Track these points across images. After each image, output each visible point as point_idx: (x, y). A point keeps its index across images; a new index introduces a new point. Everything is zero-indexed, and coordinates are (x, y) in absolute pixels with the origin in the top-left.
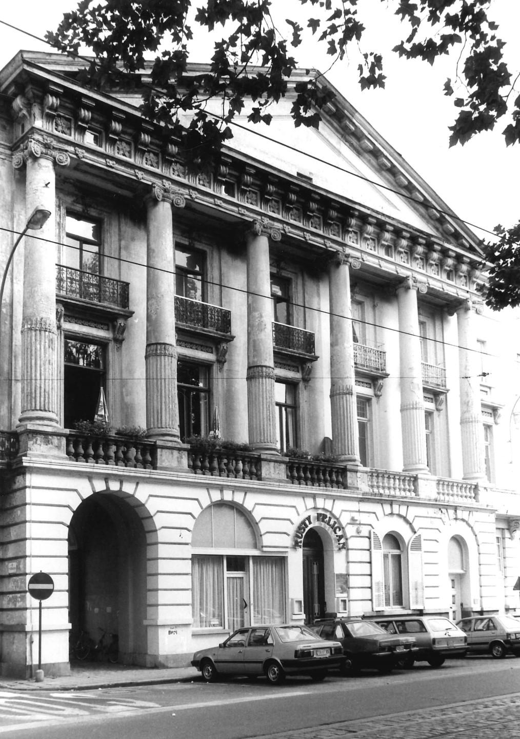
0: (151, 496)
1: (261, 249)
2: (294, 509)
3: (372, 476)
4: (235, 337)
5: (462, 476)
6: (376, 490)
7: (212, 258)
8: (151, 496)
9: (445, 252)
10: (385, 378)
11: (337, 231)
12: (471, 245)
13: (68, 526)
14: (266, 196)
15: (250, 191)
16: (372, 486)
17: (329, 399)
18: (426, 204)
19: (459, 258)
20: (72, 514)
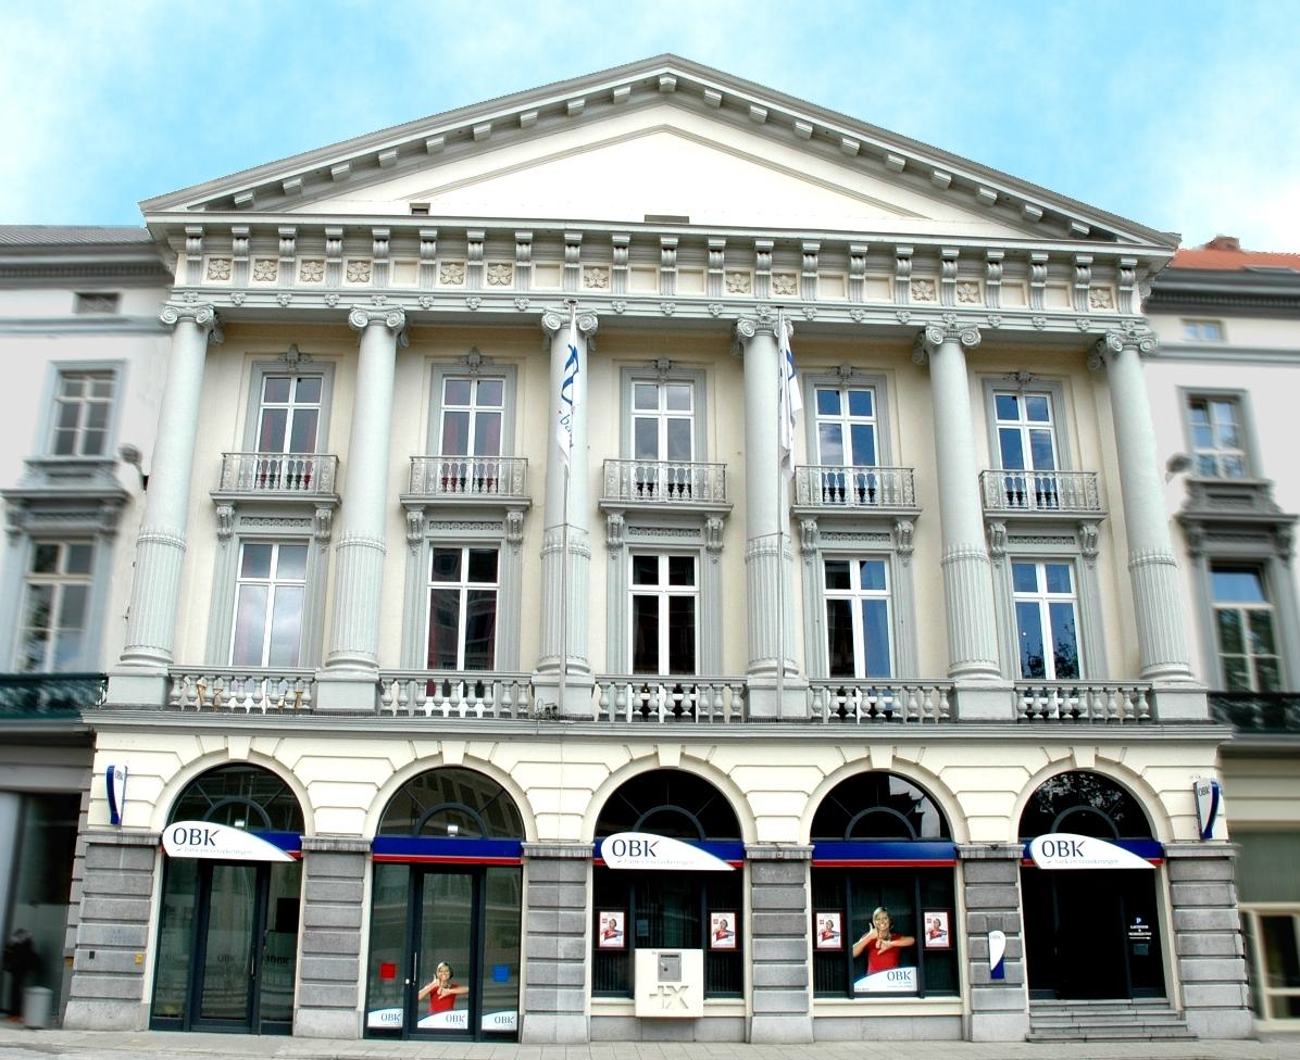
4: (1289, 521)
17: (1128, 573)
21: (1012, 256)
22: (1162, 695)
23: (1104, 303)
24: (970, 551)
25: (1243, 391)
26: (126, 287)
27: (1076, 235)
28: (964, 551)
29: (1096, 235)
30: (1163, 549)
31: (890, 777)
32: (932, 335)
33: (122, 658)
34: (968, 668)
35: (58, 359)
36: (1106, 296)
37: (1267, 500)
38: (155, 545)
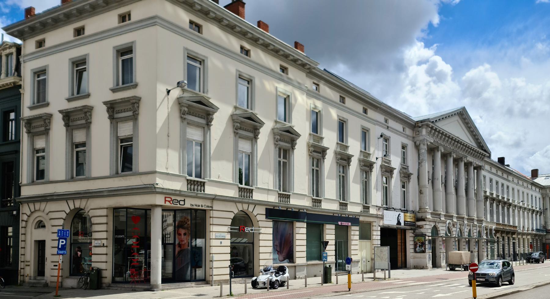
13: (232, 219)
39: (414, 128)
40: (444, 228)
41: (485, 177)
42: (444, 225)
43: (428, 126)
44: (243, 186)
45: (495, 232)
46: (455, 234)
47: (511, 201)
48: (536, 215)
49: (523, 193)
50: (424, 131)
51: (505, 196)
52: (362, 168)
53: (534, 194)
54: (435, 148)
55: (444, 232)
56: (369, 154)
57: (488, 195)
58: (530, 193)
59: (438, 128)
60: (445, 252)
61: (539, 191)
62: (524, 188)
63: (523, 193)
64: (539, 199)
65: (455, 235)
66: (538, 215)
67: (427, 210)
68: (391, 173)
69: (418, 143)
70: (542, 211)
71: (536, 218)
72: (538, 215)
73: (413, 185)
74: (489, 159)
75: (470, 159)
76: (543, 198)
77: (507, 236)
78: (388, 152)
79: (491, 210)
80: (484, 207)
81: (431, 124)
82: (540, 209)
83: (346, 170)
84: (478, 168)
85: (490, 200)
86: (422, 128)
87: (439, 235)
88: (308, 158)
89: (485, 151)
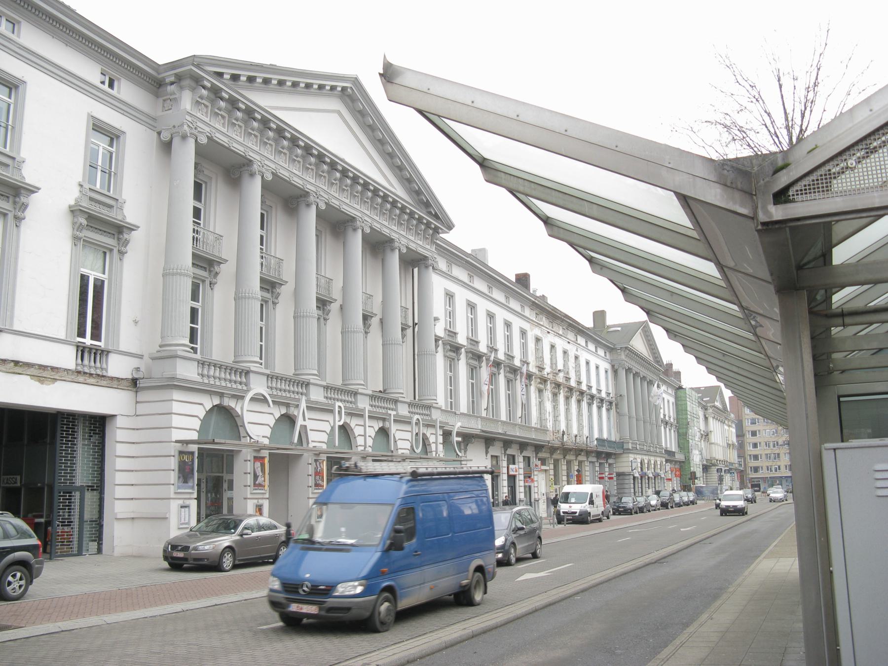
0: (356, 425)
1: (254, 189)
2: (272, 416)
3: (372, 397)
4: (32, 190)
5: (233, 359)
6: (206, 381)
7: (211, 186)
8: (356, 425)
9: (428, 225)
10: (133, 230)
11: (240, 131)
12: (436, 213)
13: (197, 431)
14: (708, 399)
15: (254, 135)
16: (203, 375)
17: (381, 346)
18: (410, 181)
19: (420, 220)
20: (200, 422)
21: (403, 209)
22: (435, 409)
23: (238, 134)
24: (184, 270)
25: (124, 133)
26: (477, 276)
27: (430, 213)
28: (173, 269)
29: (436, 217)
30: (254, 291)
31: (202, 419)
32: (255, 167)
33: (160, 346)
34: (245, 359)
35: (469, 299)
36: (205, 110)
37: (478, 346)
38: (178, 276)
39: (159, 88)
40: (408, 436)
41: (452, 296)
42: (408, 428)
43: (197, 81)
44: (88, 341)
45: (460, 439)
46: (363, 444)
47: (667, 418)
48: (599, 408)
49: (597, 368)
50: (186, 101)
51: (594, 384)
52: (448, 354)
53: (594, 361)
54: (386, 242)
55: (407, 445)
56: (455, 334)
57: (481, 350)
58: (584, 356)
59: (417, 211)
60: (195, 496)
61: (605, 356)
62: (569, 342)
63: (597, 368)
64: (606, 372)
65: (362, 448)
66: (604, 409)
67: (176, 351)
68: (323, 309)
69: (616, 367)
70: (614, 399)
71: (568, 410)
72: (604, 409)
73: (283, 313)
74: (524, 289)
75: (388, 227)
76: (615, 372)
77: (523, 455)
78: (13, 128)
79: (509, 395)
80: (260, 324)
81: (434, 222)
82: (608, 394)
83: (512, 386)
84: (651, 383)
85: (505, 370)
86: (182, 88)
87: (354, 450)
88: (467, 367)
89: (436, 217)
